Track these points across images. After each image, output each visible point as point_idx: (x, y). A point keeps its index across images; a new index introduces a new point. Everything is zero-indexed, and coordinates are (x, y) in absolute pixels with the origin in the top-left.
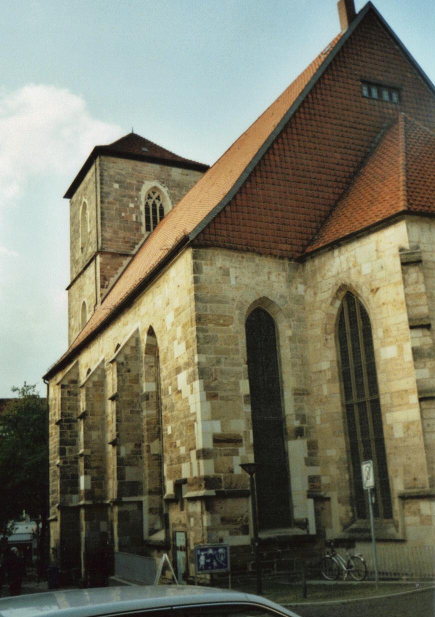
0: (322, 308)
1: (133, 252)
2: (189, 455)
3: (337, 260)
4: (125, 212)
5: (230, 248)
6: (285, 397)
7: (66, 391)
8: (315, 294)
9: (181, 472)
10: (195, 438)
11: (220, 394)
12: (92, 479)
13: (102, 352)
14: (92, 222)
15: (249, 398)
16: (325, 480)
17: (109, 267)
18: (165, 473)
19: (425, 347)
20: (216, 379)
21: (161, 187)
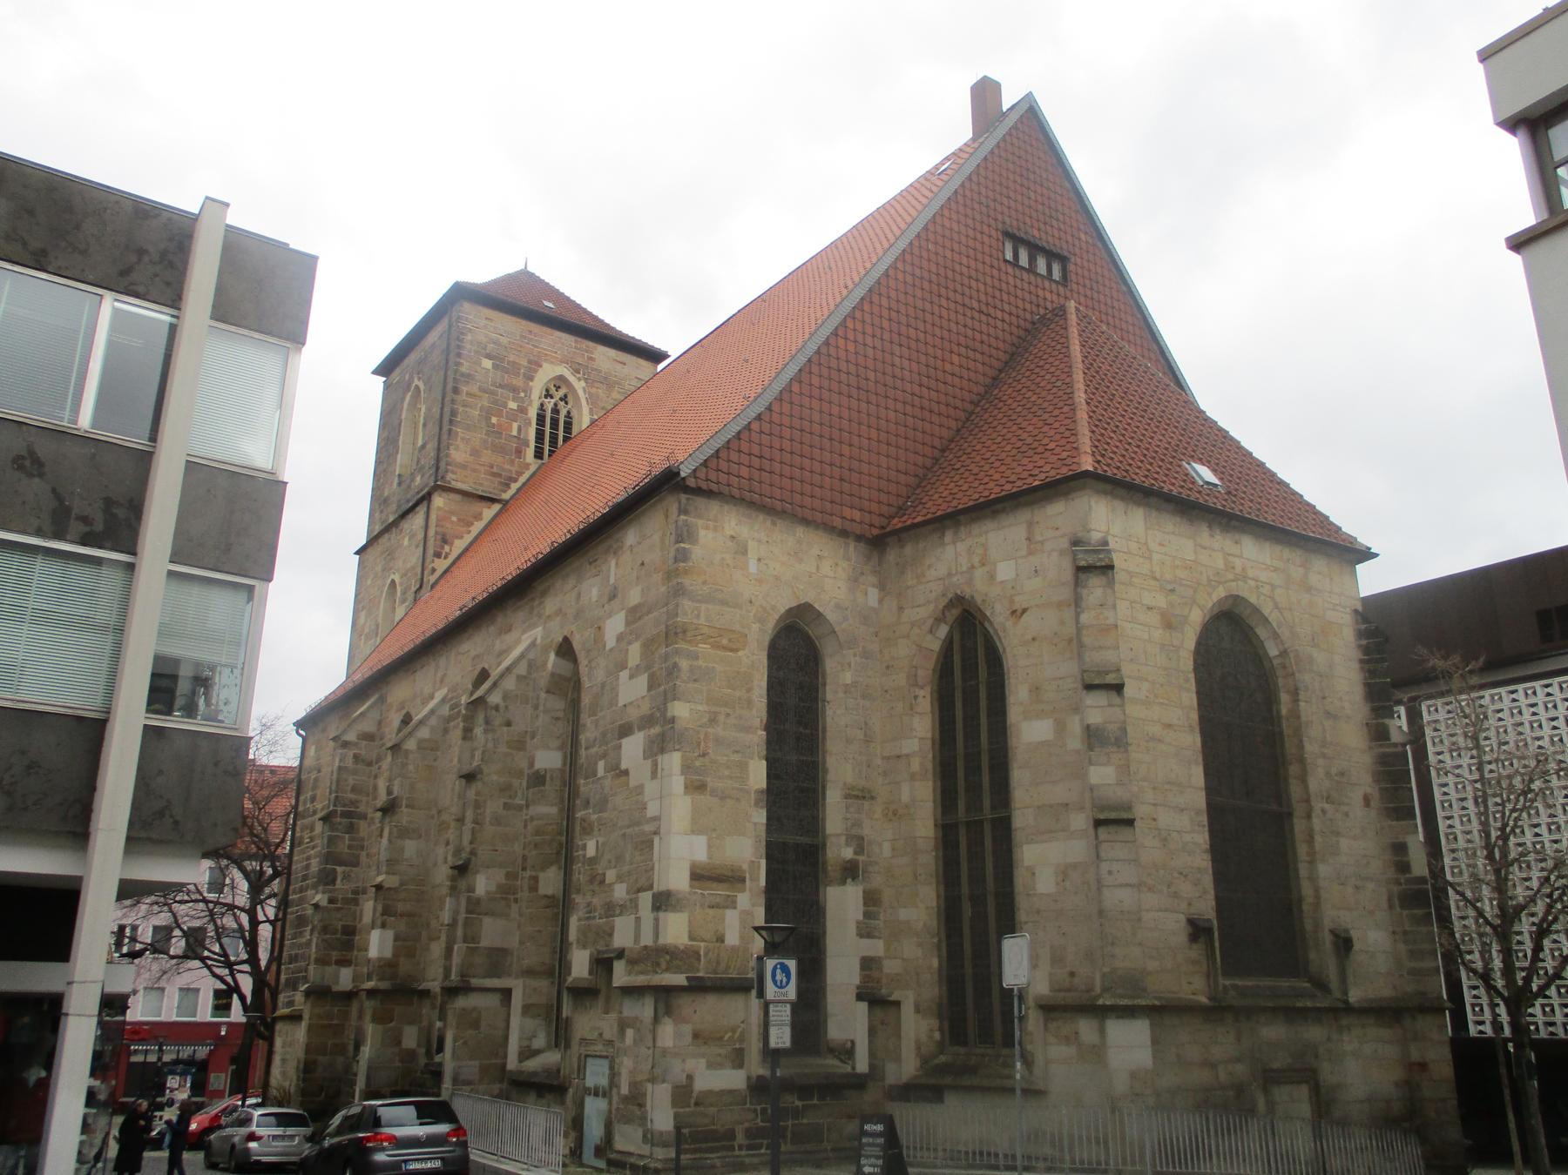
0: (920, 639)
1: (506, 496)
2: (634, 905)
3: (949, 551)
4: (499, 415)
5: (751, 504)
6: (828, 800)
7: (351, 754)
8: (901, 609)
9: (611, 935)
10: (653, 869)
11: (710, 785)
12: (396, 939)
13: (442, 681)
14: (430, 425)
15: (764, 797)
16: (891, 967)
17: (454, 519)
18: (573, 935)
19: (1110, 727)
20: (704, 755)
21: (572, 379)
